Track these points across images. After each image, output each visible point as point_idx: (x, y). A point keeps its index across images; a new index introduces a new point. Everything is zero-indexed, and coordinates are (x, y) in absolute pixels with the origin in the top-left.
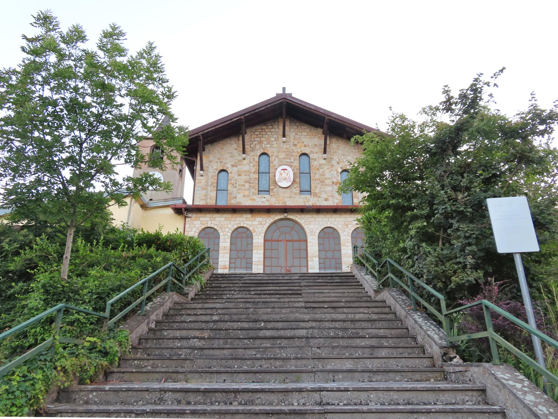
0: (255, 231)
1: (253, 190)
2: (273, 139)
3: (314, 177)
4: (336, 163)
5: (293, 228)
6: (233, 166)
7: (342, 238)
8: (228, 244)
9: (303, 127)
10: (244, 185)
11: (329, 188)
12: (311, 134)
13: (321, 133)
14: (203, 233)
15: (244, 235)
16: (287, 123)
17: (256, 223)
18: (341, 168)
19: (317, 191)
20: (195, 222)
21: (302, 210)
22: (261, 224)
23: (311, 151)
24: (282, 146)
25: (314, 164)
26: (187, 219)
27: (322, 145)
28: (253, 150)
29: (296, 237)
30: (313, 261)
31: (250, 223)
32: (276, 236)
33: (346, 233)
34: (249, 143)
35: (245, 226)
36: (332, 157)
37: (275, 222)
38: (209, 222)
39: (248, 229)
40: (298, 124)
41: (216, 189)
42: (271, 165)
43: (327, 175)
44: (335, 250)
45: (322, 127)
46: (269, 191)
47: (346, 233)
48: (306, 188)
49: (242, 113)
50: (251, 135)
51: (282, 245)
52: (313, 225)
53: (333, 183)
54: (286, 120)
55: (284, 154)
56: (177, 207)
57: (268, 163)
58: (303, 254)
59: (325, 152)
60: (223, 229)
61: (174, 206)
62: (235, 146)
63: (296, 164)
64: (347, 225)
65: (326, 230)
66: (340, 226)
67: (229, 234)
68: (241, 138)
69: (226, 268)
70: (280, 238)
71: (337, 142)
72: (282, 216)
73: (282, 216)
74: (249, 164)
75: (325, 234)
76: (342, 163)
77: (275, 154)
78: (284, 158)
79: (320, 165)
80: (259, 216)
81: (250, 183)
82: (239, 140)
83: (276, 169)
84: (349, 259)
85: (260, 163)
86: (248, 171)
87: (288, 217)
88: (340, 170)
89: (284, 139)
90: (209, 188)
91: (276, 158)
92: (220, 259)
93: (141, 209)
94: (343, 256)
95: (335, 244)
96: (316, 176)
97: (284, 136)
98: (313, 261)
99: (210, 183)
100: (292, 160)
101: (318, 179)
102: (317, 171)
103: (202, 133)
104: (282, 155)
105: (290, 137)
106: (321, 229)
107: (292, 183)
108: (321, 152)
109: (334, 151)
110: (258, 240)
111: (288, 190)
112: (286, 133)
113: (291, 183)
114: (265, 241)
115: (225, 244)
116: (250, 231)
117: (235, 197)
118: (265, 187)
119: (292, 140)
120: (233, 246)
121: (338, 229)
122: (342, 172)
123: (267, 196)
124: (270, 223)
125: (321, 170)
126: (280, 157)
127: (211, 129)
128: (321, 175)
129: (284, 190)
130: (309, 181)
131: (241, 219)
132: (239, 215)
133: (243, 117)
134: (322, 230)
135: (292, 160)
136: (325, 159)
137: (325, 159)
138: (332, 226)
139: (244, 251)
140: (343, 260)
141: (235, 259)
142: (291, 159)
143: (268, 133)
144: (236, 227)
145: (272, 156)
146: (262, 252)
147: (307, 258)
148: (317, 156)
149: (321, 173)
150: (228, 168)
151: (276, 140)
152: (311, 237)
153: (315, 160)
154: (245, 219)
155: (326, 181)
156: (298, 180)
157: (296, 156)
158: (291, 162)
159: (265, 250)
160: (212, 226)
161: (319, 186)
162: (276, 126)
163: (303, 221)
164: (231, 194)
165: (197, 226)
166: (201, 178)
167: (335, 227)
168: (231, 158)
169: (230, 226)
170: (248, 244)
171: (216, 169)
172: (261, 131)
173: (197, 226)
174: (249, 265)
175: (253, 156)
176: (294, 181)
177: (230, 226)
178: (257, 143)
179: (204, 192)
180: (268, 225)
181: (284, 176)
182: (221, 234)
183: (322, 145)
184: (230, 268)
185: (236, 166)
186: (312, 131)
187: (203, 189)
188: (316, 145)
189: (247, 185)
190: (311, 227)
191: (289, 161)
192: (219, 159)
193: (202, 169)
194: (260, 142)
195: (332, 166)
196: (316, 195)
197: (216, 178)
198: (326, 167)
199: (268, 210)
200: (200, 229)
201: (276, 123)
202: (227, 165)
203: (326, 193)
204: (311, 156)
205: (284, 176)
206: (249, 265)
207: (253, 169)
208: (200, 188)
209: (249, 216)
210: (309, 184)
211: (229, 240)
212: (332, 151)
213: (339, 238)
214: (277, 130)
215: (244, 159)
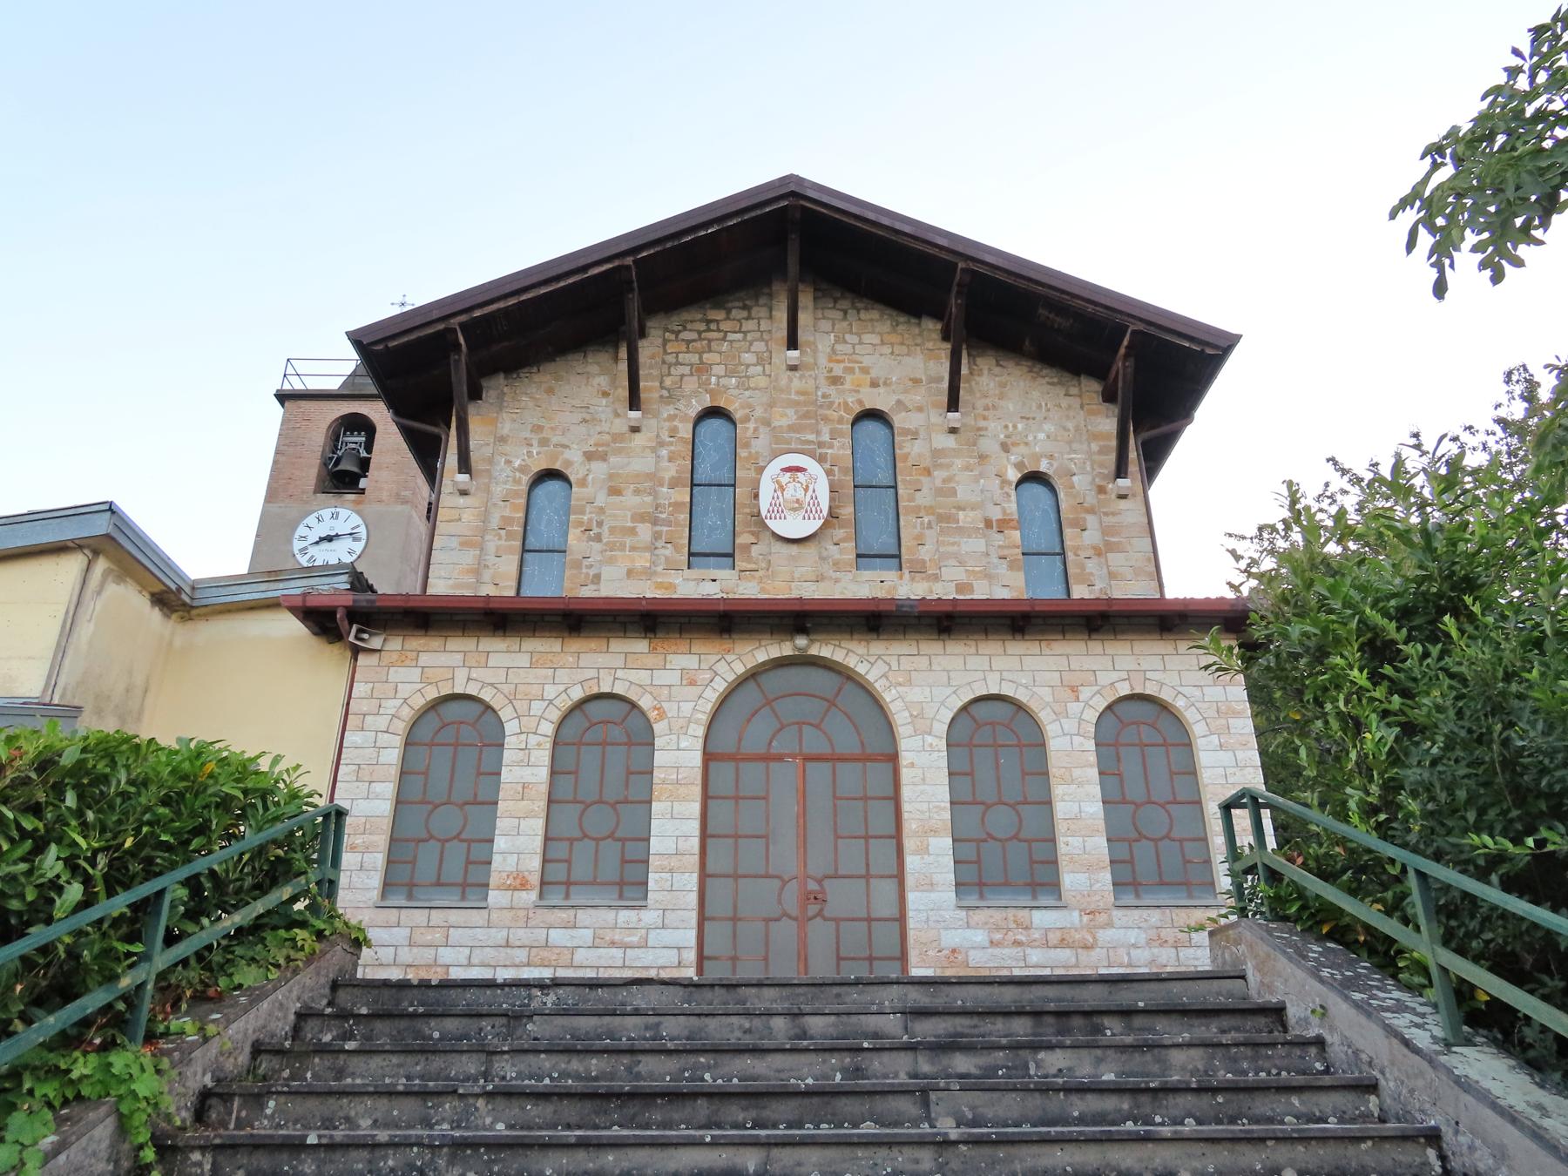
0: (662, 715)
1: (669, 551)
2: (748, 358)
3: (911, 499)
4: (997, 447)
5: (832, 703)
6: (589, 456)
7: (1056, 744)
8: (540, 774)
9: (863, 315)
10: (632, 531)
11: (975, 545)
12: (894, 338)
13: (936, 336)
14: (433, 721)
15: (616, 733)
16: (806, 299)
17: (670, 677)
18: (1019, 466)
19: (925, 553)
20: (396, 674)
21: (874, 621)
22: (692, 683)
23: (899, 402)
24: (783, 382)
25: (912, 450)
26: (363, 659)
27: (939, 380)
28: (670, 398)
29: (846, 742)
30: (924, 850)
31: (643, 677)
32: (758, 735)
33: (1070, 725)
34: (655, 372)
35: (619, 689)
36: (982, 423)
37: (753, 675)
38: (461, 675)
39: (634, 705)
40: (845, 304)
41: (518, 543)
42: (742, 453)
43: (964, 493)
44: (1025, 803)
45: (937, 315)
46: (732, 555)
47: (1070, 725)
48: (884, 542)
49: (624, 247)
50: (665, 342)
51: (784, 776)
52: (922, 689)
53: (988, 523)
54: (801, 287)
55: (791, 412)
56: (312, 602)
57: (728, 449)
58: (881, 820)
59: (953, 404)
60: (521, 706)
61: (298, 602)
62: (602, 381)
63: (841, 449)
64: (1074, 689)
65: (982, 711)
66: (1045, 693)
67: (548, 728)
68: (623, 353)
69: (524, 886)
70: (776, 747)
71: (997, 370)
72: (785, 649)
73: (785, 649)
74: (654, 450)
75: (979, 725)
76: (1022, 449)
77: (759, 412)
78: (791, 428)
79: (937, 453)
80: (683, 645)
81: (655, 522)
82: (616, 359)
83: (761, 470)
84: (1090, 842)
85: (699, 449)
86: (651, 476)
87: (814, 650)
88: (1013, 475)
89: (794, 354)
90: (492, 544)
91: (763, 430)
92: (500, 843)
93: (156, 614)
94: (1061, 827)
95: (1024, 774)
96: (917, 495)
97: (792, 343)
98: (924, 850)
99: (495, 522)
100: (826, 437)
101: (930, 510)
102: (925, 480)
103: (463, 318)
104: (785, 418)
105: (815, 351)
106: (960, 704)
107: (826, 525)
108: (935, 405)
109: (988, 401)
110: (678, 754)
111: (810, 551)
112: (802, 336)
113: (819, 523)
114: (708, 757)
115: (527, 774)
116: (643, 713)
117: (597, 579)
118: (721, 543)
119: (823, 361)
120: (566, 783)
121: (1034, 705)
122: (1020, 483)
123: (724, 574)
124: (731, 677)
125: (939, 475)
126: (776, 423)
127: (501, 305)
128: (940, 492)
129: (794, 549)
130: (892, 515)
131: (601, 659)
132: (593, 644)
133: (629, 261)
134: (964, 709)
135: (826, 437)
136: (953, 431)
137: (953, 431)
138: (1007, 690)
139: (613, 805)
140: (1062, 848)
141: (571, 840)
142: (818, 433)
143: (731, 336)
144: (577, 694)
145: (747, 419)
146: (695, 808)
147: (898, 836)
148: (922, 423)
149: (938, 483)
150: (569, 463)
151: (760, 361)
152: (916, 742)
153: (915, 435)
154: (618, 661)
155: (961, 515)
156: (847, 511)
157: (841, 420)
158: (821, 445)
159: (706, 797)
160: (472, 690)
161: (931, 536)
162: (763, 312)
163: (880, 668)
164: (577, 565)
165: (404, 691)
166: (462, 501)
167: (1022, 696)
168: (583, 428)
169: (550, 691)
170: (630, 773)
171: (522, 469)
172: (702, 327)
173: (404, 691)
174: (632, 872)
175: (670, 419)
176: (832, 515)
177: (550, 691)
178: (687, 370)
179: (469, 557)
180: (721, 686)
181: (793, 492)
182: (511, 727)
183: (939, 380)
184: (543, 883)
185: (603, 457)
186: (901, 328)
187: (466, 544)
188: (916, 381)
189: (645, 531)
190: (916, 694)
191: (812, 437)
192: (538, 429)
193: (465, 465)
194: (702, 369)
195: (982, 457)
196: (919, 570)
197: (523, 501)
198: (959, 463)
199: (725, 621)
200: (419, 702)
201: (762, 301)
202: (567, 454)
203: (962, 563)
204: (898, 420)
205: (793, 492)
206: (632, 872)
207: (670, 471)
208: (454, 542)
209: (640, 645)
210: (892, 528)
211: (543, 756)
212: (980, 403)
213: (1039, 745)
214: (764, 325)
215: (635, 430)
